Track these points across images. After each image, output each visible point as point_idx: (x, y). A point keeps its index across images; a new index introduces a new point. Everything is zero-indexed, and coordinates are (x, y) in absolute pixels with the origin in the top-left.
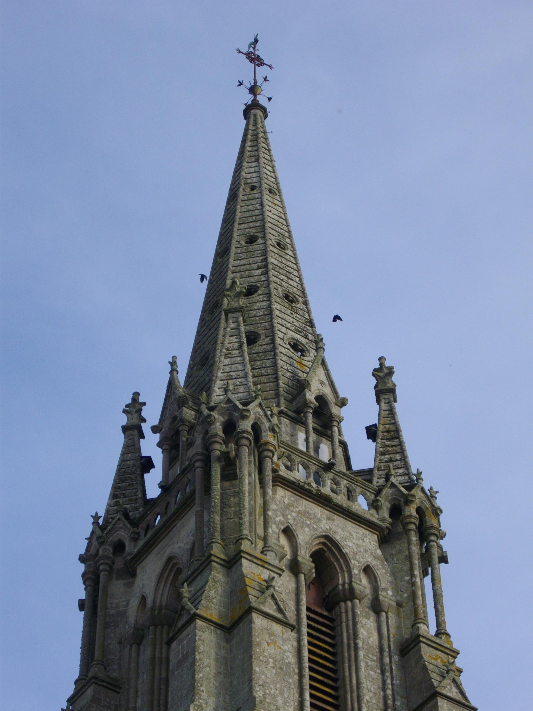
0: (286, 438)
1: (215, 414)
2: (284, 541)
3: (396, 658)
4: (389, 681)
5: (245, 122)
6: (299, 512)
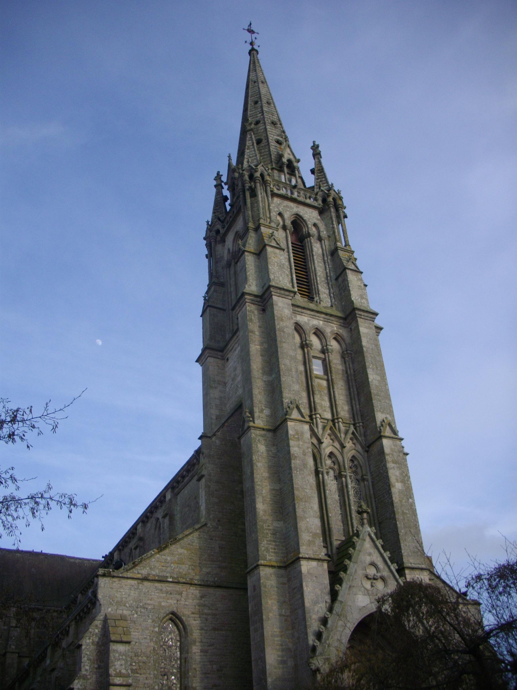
0: (277, 178)
1: (245, 172)
2: (279, 218)
3: (329, 257)
4: (327, 266)
5: (249, 57)
6: (284, 206)
